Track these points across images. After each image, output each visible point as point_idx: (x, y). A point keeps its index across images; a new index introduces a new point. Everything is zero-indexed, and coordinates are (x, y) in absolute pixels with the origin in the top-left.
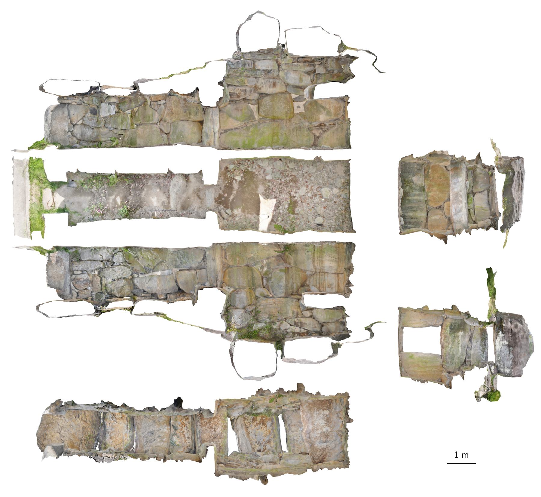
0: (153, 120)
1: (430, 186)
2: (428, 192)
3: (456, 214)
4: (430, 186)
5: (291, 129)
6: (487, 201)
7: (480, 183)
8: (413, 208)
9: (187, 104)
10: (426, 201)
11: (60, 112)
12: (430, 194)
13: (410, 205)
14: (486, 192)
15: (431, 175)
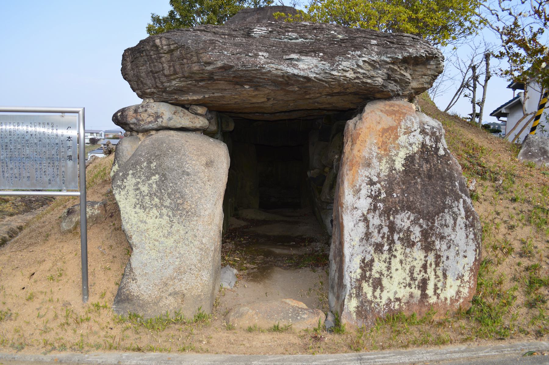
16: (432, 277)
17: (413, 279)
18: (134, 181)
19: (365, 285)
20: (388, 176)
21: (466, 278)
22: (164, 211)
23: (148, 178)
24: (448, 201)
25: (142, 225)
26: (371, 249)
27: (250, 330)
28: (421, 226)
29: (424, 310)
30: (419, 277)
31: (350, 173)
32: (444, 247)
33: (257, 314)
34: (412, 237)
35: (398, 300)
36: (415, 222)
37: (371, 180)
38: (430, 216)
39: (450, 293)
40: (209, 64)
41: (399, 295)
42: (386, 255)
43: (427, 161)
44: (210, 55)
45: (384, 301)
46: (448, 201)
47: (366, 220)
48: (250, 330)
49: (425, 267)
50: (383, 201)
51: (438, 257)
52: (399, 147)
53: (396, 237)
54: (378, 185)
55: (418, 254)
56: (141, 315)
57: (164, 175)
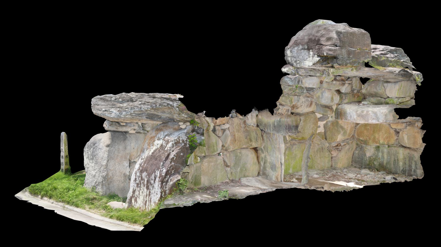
0: (217, 150)
1: (374, 141)
2: (379, 143)
3: (378, 119)
4: (374, 141)
5: (316, 150)
6: (393, 84)
7: (375, 90)
8: (395, 160)
9: (247, 128)
10: (389, 146)
11: (121, 147)
12: (381, 142)
13: (392, 163)
14: (385, 85)
15: (365, 138)
26: (136, 185)
47: (136, 173)
51: (150, 192)
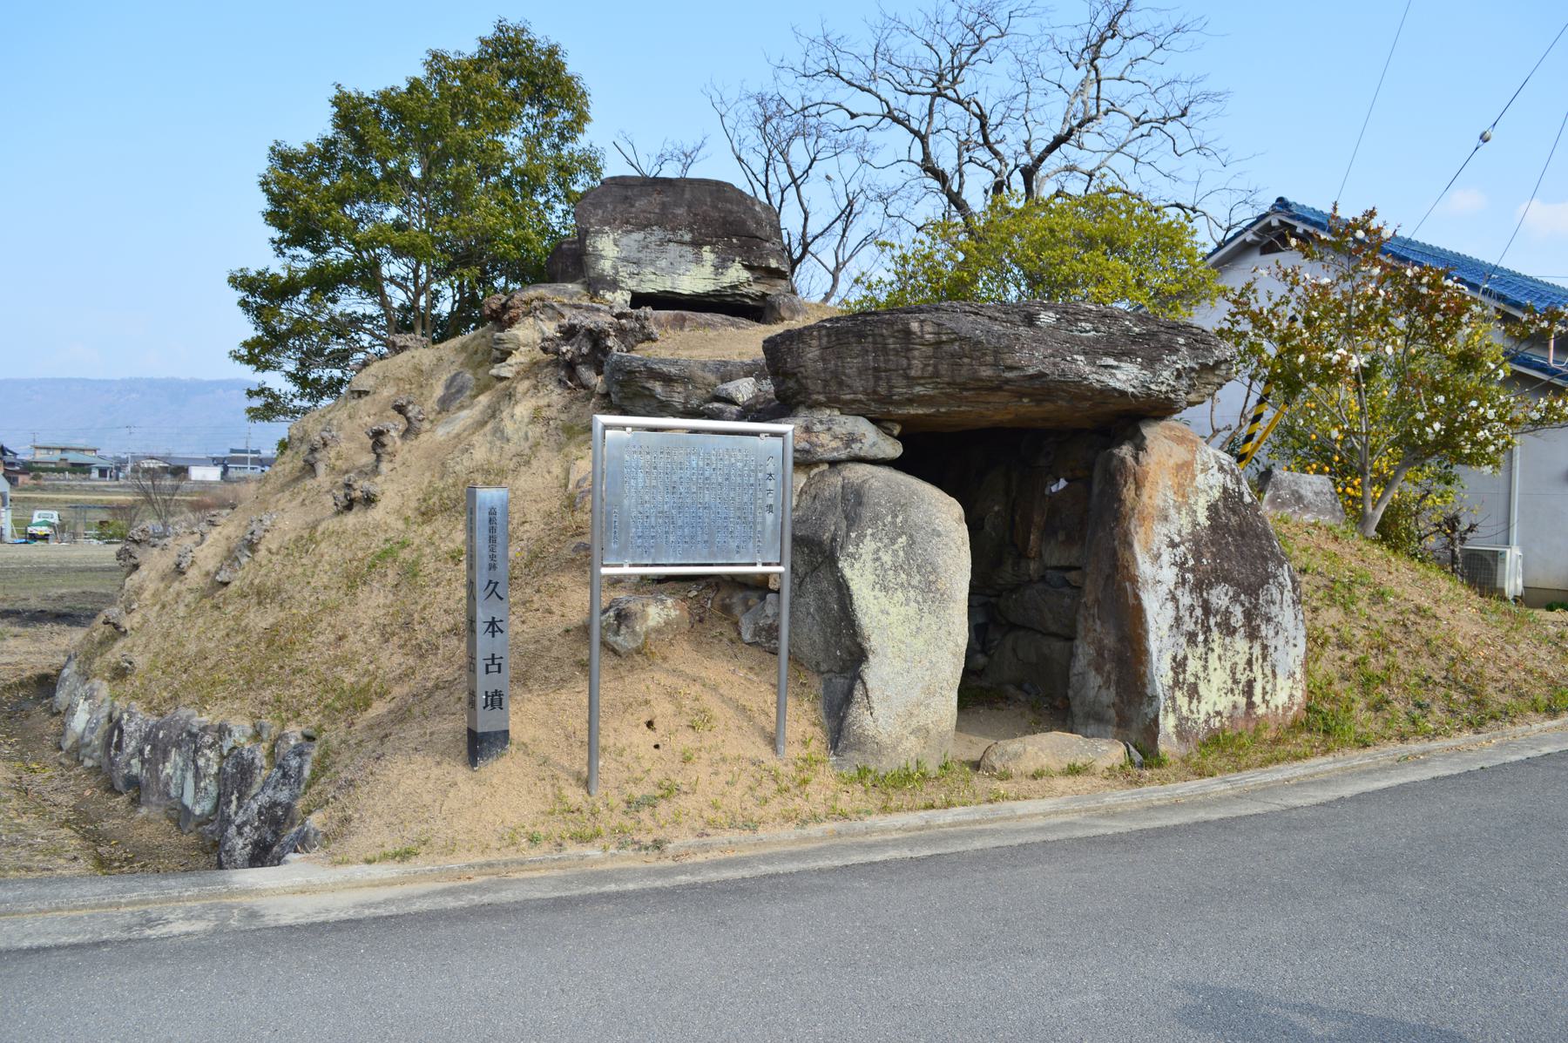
16: (1260, 677)
17: (1236, 682)
18: (873, 546)
19: (1178, 694)
20: (1192, 533)
21: (1298, 676)
22: (912, 594)
23: (893, 541)
24: (1271, 567)
25: (883, 618)
26: (1183, 640)
27: (1035, 776)
28: (1243, 605)
29: (1252, 725)
30: (1244, 679)
31: (1141, 530)
32: (1271, 633)
33: (1041, 749)
34: (1232, 621)
35: (1218, 713)
36: (1235, 599)
37: (1172, 540)
38: (1251, 588)
39: (1281, 699)
40: (1011, 368)
41: (1219, 708)
42: (1201, 649)
43: (1235, 512)
44: (1020, 357)
45: (1203, 717)
46: (1271, 567)
47: (1174, 599)
48: (1035, 776)
49: (1250, 663)
50: (1192, 570)
51: (1265, 647)
52: (1197, 491)
53: (1212, 621)
54: (1182, 548)
55: (1241, 644)
56: (873, 768)
57: (911, 536)
